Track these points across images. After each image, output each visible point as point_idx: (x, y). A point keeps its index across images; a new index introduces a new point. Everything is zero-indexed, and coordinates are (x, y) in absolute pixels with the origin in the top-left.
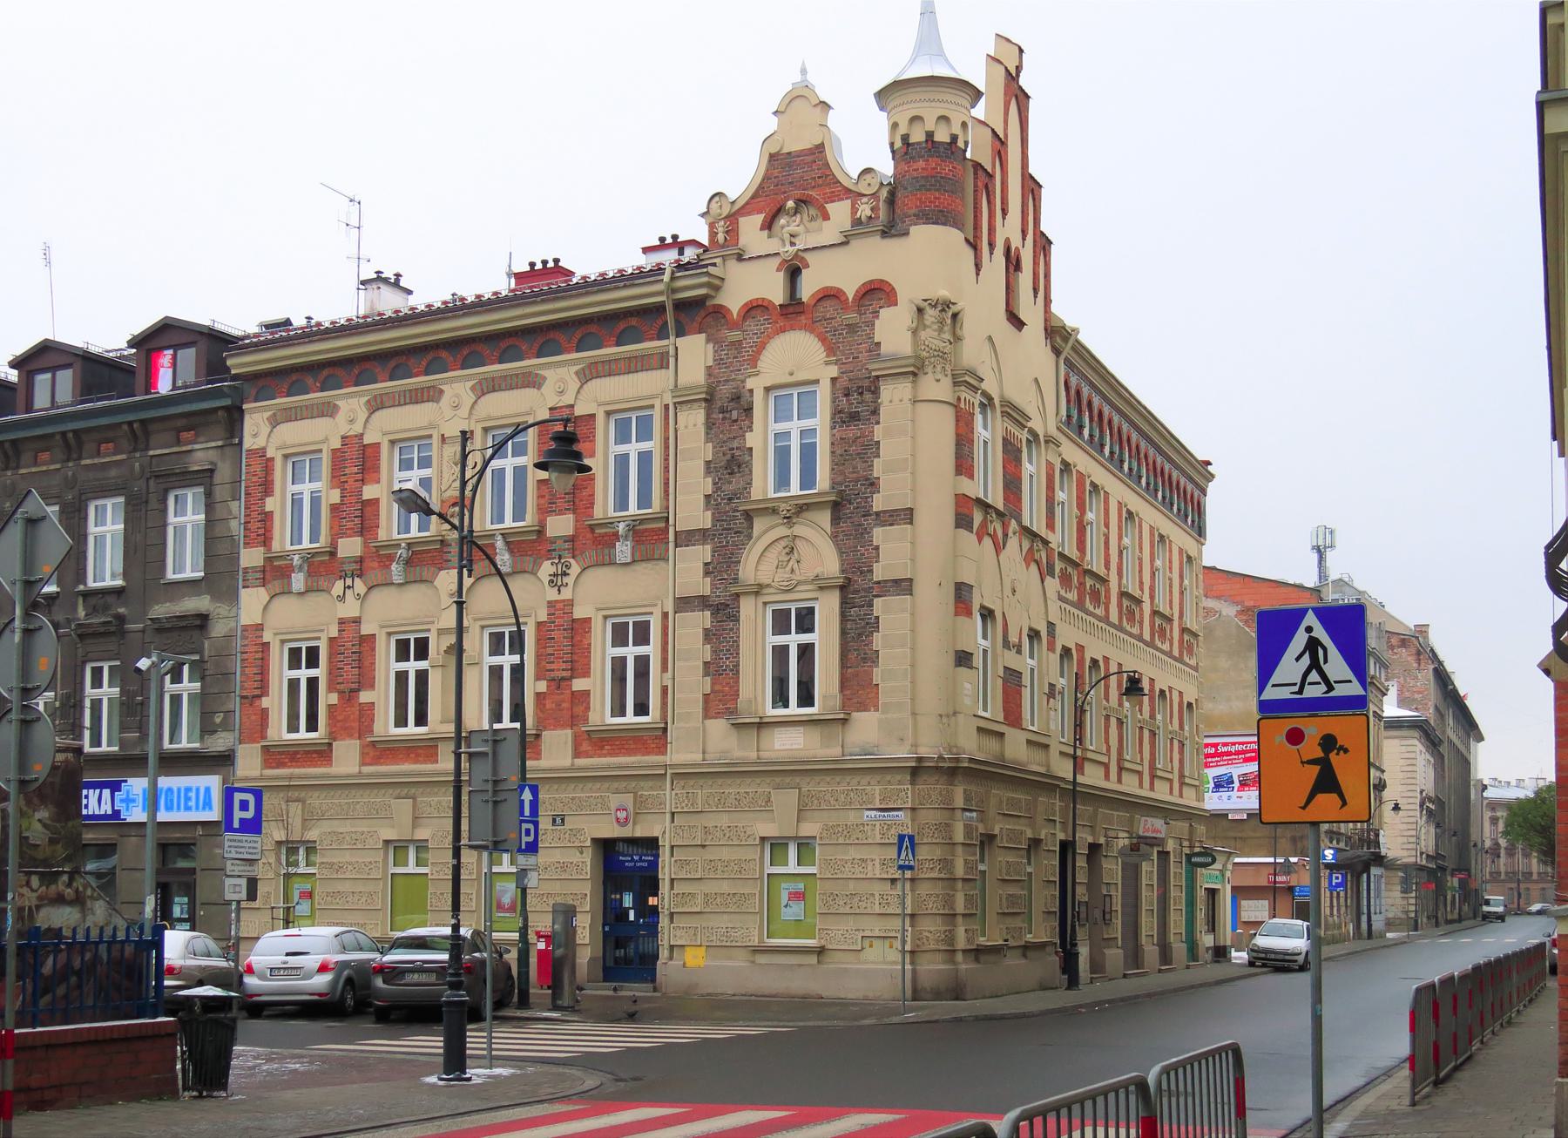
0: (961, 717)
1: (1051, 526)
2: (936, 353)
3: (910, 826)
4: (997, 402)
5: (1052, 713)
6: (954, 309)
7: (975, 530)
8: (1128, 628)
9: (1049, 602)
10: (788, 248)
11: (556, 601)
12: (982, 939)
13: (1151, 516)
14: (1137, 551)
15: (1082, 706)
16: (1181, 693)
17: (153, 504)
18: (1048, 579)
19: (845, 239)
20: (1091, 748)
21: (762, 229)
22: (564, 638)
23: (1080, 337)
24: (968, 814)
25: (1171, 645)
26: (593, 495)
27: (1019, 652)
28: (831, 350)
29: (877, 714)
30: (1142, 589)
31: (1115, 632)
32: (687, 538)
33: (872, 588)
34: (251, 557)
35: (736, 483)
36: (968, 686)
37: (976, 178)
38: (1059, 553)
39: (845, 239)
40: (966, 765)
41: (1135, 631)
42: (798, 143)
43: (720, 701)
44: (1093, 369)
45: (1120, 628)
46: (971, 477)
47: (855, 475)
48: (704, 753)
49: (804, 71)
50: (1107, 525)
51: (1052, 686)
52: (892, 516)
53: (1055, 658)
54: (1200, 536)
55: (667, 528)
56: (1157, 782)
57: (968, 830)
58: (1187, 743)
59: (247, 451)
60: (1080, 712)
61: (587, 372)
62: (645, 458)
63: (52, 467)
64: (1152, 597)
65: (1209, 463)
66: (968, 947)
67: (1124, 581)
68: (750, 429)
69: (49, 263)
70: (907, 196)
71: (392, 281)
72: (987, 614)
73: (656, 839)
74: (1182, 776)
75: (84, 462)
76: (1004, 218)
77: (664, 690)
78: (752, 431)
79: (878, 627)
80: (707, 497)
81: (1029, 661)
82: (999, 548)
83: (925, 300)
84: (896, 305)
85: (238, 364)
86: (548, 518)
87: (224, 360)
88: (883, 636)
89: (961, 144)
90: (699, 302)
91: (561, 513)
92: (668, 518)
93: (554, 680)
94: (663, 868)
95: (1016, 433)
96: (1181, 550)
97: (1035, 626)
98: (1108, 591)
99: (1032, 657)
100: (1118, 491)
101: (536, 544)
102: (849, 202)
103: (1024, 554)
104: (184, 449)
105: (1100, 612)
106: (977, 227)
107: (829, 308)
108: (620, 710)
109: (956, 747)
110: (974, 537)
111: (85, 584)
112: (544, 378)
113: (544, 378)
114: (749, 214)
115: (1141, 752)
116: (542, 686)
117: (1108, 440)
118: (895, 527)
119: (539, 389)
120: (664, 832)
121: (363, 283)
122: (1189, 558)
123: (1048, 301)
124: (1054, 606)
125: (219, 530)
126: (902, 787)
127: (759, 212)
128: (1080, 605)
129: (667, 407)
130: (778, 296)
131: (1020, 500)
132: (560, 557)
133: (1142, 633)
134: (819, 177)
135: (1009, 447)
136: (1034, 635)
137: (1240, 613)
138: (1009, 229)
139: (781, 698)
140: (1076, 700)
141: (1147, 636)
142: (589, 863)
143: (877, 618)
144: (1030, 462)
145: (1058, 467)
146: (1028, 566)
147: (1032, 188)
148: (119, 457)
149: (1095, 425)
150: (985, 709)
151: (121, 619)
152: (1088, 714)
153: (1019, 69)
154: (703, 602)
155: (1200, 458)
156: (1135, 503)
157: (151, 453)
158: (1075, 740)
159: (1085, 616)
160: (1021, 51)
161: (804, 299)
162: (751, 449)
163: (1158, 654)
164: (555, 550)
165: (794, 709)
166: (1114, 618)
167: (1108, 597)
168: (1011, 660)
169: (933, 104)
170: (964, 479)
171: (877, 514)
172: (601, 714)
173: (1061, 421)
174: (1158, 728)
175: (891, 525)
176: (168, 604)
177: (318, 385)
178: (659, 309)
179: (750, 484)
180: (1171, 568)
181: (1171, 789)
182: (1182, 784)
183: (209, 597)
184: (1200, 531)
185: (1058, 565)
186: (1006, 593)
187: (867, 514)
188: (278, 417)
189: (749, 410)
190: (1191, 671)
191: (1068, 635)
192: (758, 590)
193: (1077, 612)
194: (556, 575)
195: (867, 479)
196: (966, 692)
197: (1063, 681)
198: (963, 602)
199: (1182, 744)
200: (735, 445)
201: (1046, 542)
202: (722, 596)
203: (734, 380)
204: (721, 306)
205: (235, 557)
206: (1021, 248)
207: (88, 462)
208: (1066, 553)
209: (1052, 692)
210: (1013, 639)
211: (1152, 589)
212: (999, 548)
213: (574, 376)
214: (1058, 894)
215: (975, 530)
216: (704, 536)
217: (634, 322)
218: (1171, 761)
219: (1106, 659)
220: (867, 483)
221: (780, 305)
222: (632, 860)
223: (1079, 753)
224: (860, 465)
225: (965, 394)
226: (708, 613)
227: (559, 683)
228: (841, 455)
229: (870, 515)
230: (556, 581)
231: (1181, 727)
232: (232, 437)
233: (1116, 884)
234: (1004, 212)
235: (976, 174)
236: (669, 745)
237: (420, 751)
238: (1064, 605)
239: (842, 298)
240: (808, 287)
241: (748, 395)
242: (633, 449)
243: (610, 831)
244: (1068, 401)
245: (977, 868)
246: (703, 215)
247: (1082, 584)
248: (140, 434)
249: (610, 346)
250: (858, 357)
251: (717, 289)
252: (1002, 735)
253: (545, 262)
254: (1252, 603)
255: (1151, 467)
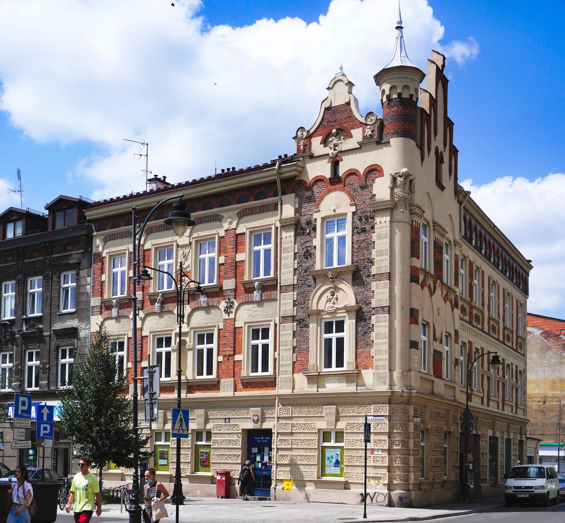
0: (413, 373)
1: (457, 284)
2: (402, 199)
3: (388, 424)
4: (431, 223)
5: (456, 372)
6: (410, 178)
7: (420, 284)
8: (492, 334)
9: (455, 319)
10: (332, 151)
11: (227, 319)
12: (445, 477)
13: (503, 283)
14: (497, 299)
15: (471, 370)
16: (517, 366)
17: (55, 278)
18: (455, 309)
19: (359, 146)
20: (475, 389)
21: (321, 144)
22: (231, 336)
23: (471, 196)
24: (415, 419)
25: (512, 344)
26: (244, 270)
27: (441, 342)
28: (352, 198)
29: (373, 370)
30: (499, 317)
31: (487, 336)
32: (285, 288)
33: (371, 311)
34: (95, 302)
35: (309, 263)
36: (416, 357)
37: (422, 116)
38: (460, 297)
39: (359, 146)
40: (415, 395)
41: (496, 336)
42: (339, 101)
43: (300, 364)
44: (477, 212)
45: (488, 334)
46: (418, 258)
47: (363, 258)
48: (293, 389)
49: (341, 68)
50: (483, 286)
51: (457, 360)
52: (381, 276)
53: (458, 347)
54: (526, 294)
55: (277, 285)
56: (505, 406)
57: (416, 426)
58: (519, 389)
59: (94, 254)
60: (469, 374)
61: (242, 213)
62: (267, 252)
63: (12, 263)
64: (504, 321)
65: (530, 261)
66: (415, 483)
67: (491, 312)
68: (315, 237)
69: (20, 178)
70: (389, 124)
71: (162, 179)
72: (426, 325)
73: (271, 430)
74: (517, 404)
75: (26, 261)
76: (435, 137)
77: (275, 360)
78: (316, 238)
79: (373, 329)
80: (295, 270)
81: (446, 347)
82: (432, 293)
83: (397, 174)
84: (383, 176)
85: (90, 214)
86: (224, 281)
87: (84, 213)
88: (376, 333)
89: (414, 99)
90: (292, 179)
91: (230, 278)
92: (277, 280)
93: (226, 356)
94: (274, 443)
95: (440, 239)
96: (517, 301)
97: (449, 331)
98: (483, 317)
99: (447, 346)
100: (488, 270)
101: (219, 293)
102: (361, 129)
103: (444, 297)
104: (68, 254)
105: (480, 326)
106: (422, 139)
107: (352, 179)
108: (255, 369)
109: (410, 386)
110: (420, 287)
111: (26, 315)
112: (223, 217)
113: (223, 217)
114: (315, 136)
115: (498, 392)
116: (221, 358)
117: (484, 246)
118: (382, 282)
119: (220, 222)
120: (275, 426)
121: (149, 180)
122: (521, 304)
123: (456, 179)
124: (458, 322)
125: (82, 290)
126: (384, 405)
127: (320, 135)
128: (470, 323)
129: (277, 228)
130: (328, 174)
131: (442, 271)
132: (229, 299)
133: (499, 337)
134: (348, 118)
135: (437, 245)
136: (448, 336)
137: (542, 334)
138: (438, 142)
139: (328, 364)
140: (468, 366)
141: (501, 339)
142: (240, 441)
143: (373, 325)
144: (447, 254)
145: (460, 257)
146: (445, 302)
147: (449, 124)
148: (40, 258)
149: (478, 239)
150: (425, 369)
151: (41, 330)
152: (474, 374)
153: (443, 66)
154: (293, 318)
155: (527, 259)
156: (497, 276)
157: (54, 256)
158: (468, 385)
159: (472, 328)
160: (444, 58)
161: (340, 175)
162: (315, 247)
163: (506, 347)
164: (227, 296)
165: (334, 368)
166: (486, 329)
167: (483, 320)
168: (437, 346)
169: (401, 80)
170: (415, 259)
171: (374, 275)
172: (245, 372)
173: (462, 236)
174: (506, 382)
175: (380, 280)
176: (60, 323)
177: (124, 223)
178: (274, 182)
179: (315, 263)
180: (512, 308)
181: (512, 410)
182: (517, 408)
183: (77, 320)
184: (525, 291)
185: (460, 303)
186: (435, 315)
187: (369, 276)
188: (107, 238)
189: (314, 229)
190: (522, 356)
191: (465, 336)
192: (319, 313)
193: (469, 325)
194: (227, 307)
195: (369, 259)
196: (415, 360)
197: (462, 358)
198: (414, 317)
199: (517, 390)
200: (308, 244)
201: (455, 292)
202: (301, 315)
203: (308, 215)
204: (302, 180)
205: (88, 302)
206: (443, 151)
207: (27, 261)
208: (464, 297)
209: (457, 362)
210: (438, 335)
211: (504, 317)
212: (432, 293)
213: (236, 216)
214: (459, 457)
215: (420, 284)
216: (294, 287)
217: (262, 189)
218: (512, 397)
219: (482, 349)
220: (369, 261)
221: (329, 179)
222: (261, 439)
223: (469, 392)
224: (366, 252)
225: (416, 219)
226: (295, 324)
227: (228, 357)
228: (357, 249)
229: (371, 276)
230: (227, 311)
231: (517, 382)
232: (88, 248)
233: (487, 453)
234: (436, 134)
235: (421, 114)
236: (277, 386)
237: (167, 389)
238: (463, 322)
239: (358, 174)
240: (342, 169)
241: (314, 221)
242: (262, 248)
243: (250, 425)
244: (465, 227)
245: (420, 444)
246: (294, 138)
247: (471, 313)
248: (49, 248)
249: (252, 201)
250: (365, 202)
251: (301, 172)
252: (433, 381)
253: (228, 169)
254: (548, 329)
255: (504, 261)
